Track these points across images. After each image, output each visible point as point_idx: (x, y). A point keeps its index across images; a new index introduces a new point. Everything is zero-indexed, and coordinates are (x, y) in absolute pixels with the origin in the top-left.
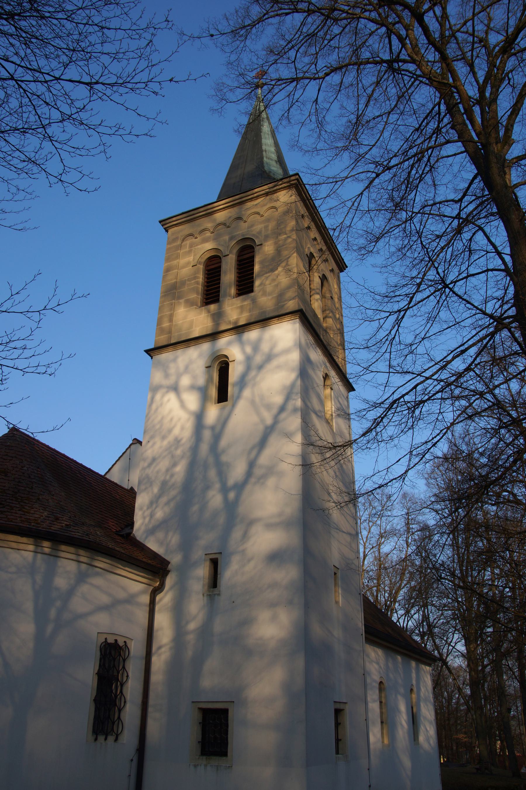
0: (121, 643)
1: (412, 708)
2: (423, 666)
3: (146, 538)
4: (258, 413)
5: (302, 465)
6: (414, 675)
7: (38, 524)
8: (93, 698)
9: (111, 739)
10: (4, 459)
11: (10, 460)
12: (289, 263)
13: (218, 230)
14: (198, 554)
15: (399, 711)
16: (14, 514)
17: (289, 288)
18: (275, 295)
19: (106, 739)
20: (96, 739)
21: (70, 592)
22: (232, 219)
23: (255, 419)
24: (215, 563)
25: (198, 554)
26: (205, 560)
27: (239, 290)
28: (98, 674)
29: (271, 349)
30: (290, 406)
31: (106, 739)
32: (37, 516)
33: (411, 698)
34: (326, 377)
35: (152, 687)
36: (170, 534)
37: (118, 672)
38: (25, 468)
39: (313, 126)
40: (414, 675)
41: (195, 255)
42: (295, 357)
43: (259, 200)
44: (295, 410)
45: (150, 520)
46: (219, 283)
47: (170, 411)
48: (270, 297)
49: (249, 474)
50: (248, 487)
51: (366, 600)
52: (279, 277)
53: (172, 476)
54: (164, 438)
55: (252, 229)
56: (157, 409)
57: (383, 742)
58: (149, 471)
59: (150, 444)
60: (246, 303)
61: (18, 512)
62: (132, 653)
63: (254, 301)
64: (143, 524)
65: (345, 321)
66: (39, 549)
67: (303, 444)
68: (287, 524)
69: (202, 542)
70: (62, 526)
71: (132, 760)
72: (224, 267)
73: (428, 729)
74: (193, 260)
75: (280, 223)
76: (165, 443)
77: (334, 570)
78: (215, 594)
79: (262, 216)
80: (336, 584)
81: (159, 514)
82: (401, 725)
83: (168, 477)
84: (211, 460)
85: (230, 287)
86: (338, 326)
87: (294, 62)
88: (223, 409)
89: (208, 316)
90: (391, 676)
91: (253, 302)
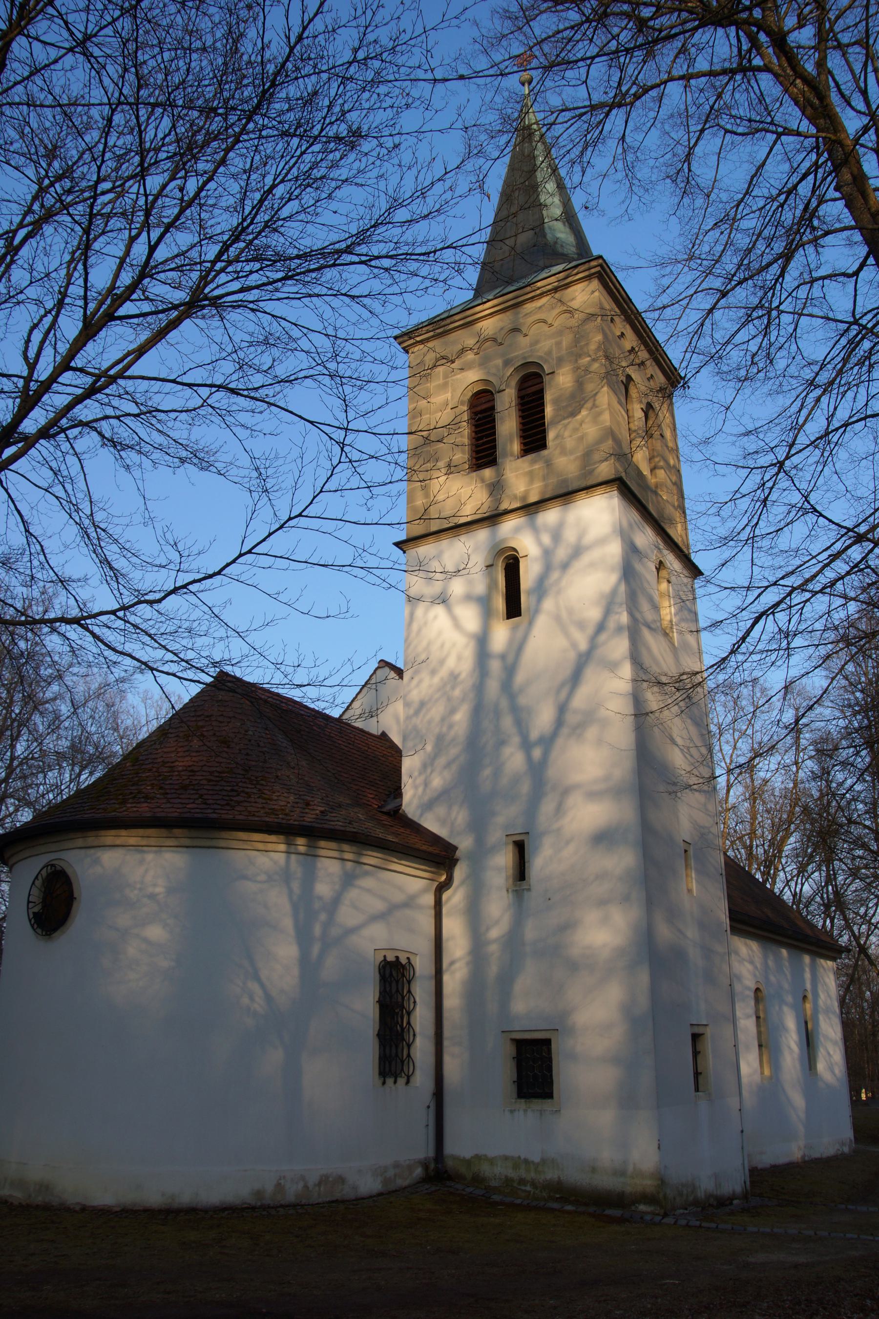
0: (403, 961)
1: (806, 1023)
2: (822, 961)
3: (421, 815)
4: (566, 633)
5: (635, 715)
6: (808, 975)
7: (286, 815)
8: (376, 1033)
9: (401, 1081)
10: (221, 722)
11: (229, 722)
12: (597, 402)
13: (485, 350)
14: (496, 835)
15: (786, 1029)
16: (254, 805)
17: (600, 441)
18: (579, 454)
19: (395, 1082)
20: (384, 1083)
21: (336, 901)
22: (504, 332)
23: (561, 642)
24: (520, 847)
25: (496, 835)
26: (506, 844)
27: (525, 444)
28: (379, 1002)
29: (580, 537)
30: (611, 624)
31: (395, 1082)
32: (283, 803)
33: (805, 1010)
34: (660, 566)
35: (446, 1014)
36: (455, 808)
37: (403, 998)
38: (250, 733)
39: (620, 175)
40: (808, 975)
41: (454, 390)
42: (614, 550)
43: (544, 300)
44: (619, 629)
45: (424, 790)
46: (494, 434)
47: (440, 633)
48: (572, 457)
49: (559, 722)
50: (560, 741)
51: (732, 867)
52: (583, 426)
53: (451, 727)
54: (433, 672)
55: (538, 347)
56: (419, 631)
57: (762, 1073)
58: (417, 721)
59: (415, 682)
60: (537, 466)
61: (258, 800)
62: (418, 973)
63: (549, 464)
64: (414, 796)
65: (685, 469)
66: (292, 849)
67: (634, 681)
68: (616, 792)
69: (500, 820)
70: (317, 815)
71: (428, 1107)
72: (499, 407)
73: (832, 1053)
74: (452, 399)
75: (579, 337)
76: (436, 680)
77: (683, 846)
78: (523, 890)
79: (551, 325)
80: (687, 866)
81: (437, 782)
82: (789, 1048)
83: (444, 729)
84: (504, 704)
85: (511, 442)
86: (674, 479)
87: (586, 82)
88: (514, 629)
89: (482, 487)
90: (772, 979)
91: (548, 465)
